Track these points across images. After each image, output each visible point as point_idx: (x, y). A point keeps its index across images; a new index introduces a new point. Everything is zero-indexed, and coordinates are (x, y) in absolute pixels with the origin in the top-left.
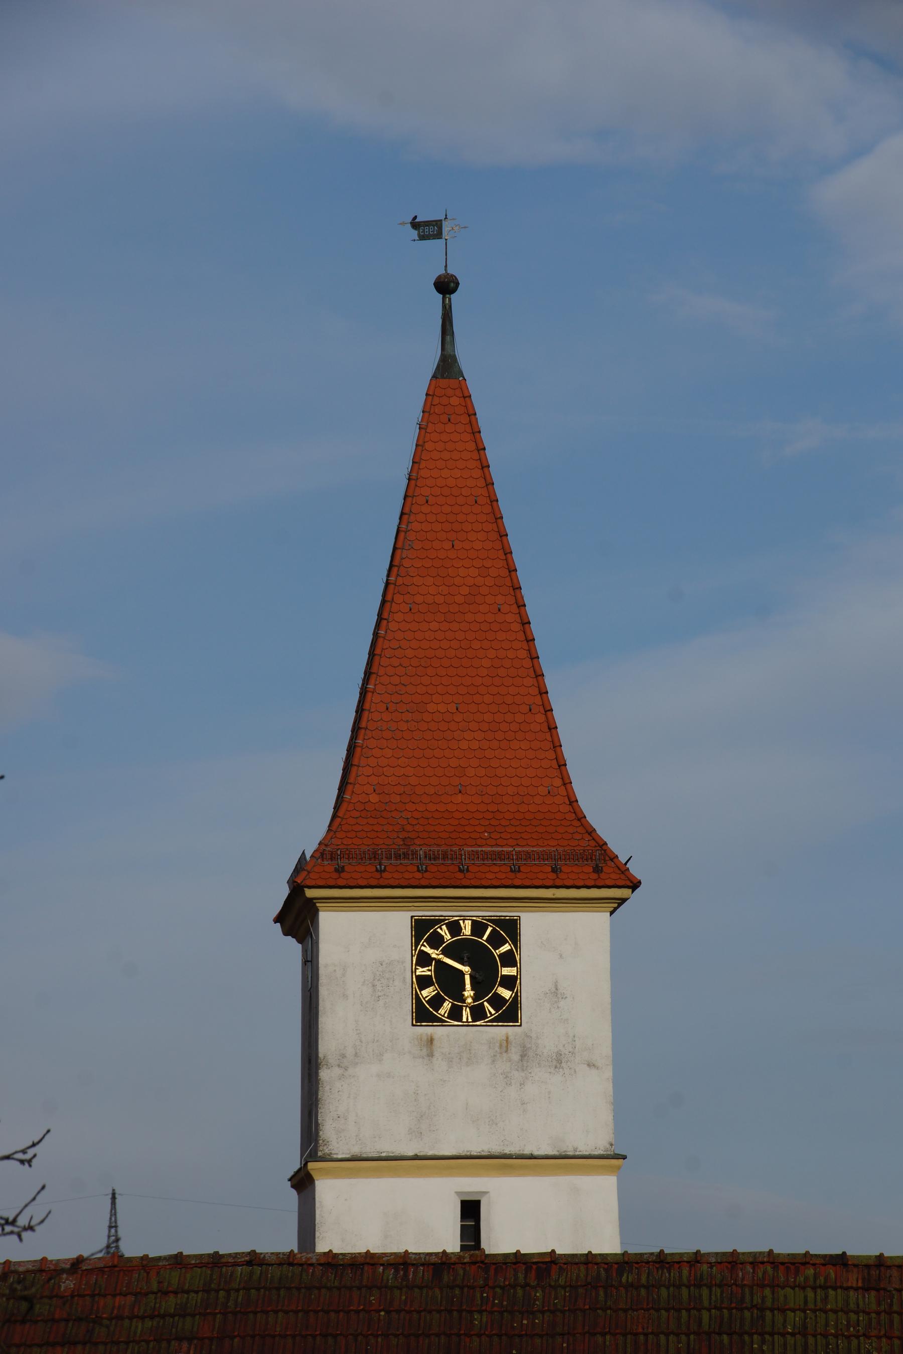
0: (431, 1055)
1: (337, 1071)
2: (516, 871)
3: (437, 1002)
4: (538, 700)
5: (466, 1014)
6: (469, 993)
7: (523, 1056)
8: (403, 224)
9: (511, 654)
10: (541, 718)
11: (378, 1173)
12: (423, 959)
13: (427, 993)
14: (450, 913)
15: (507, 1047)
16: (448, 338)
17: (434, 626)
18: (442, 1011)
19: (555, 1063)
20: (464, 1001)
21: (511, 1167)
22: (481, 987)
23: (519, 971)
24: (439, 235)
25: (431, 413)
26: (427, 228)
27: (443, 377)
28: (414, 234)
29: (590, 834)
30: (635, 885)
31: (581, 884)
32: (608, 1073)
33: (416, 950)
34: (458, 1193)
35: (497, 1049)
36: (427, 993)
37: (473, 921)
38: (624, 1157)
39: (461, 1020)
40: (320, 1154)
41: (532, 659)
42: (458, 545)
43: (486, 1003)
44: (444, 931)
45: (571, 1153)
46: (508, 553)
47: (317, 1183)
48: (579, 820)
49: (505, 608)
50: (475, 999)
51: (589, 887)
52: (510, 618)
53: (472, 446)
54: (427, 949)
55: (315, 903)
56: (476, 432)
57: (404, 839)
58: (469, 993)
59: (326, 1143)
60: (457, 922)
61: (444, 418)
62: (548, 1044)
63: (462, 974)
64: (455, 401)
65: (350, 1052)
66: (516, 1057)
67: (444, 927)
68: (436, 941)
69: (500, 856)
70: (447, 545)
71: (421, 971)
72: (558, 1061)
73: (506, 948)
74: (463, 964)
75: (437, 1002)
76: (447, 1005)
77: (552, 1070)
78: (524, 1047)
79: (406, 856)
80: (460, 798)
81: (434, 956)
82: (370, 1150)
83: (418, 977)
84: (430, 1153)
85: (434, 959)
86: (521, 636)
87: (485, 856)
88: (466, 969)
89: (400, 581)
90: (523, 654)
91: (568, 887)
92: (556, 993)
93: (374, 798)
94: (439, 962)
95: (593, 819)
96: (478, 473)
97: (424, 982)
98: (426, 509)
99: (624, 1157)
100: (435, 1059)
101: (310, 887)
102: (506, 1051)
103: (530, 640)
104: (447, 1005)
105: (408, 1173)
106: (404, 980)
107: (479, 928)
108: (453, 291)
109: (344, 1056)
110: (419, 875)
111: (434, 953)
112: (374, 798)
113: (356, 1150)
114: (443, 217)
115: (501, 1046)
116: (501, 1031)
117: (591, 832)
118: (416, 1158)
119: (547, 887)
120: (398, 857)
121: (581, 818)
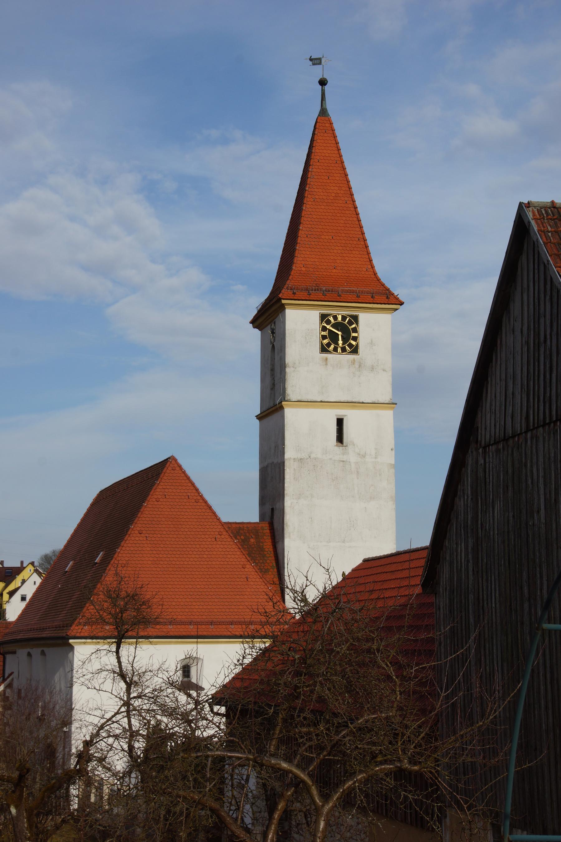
0: (326, 364)
1: (292, 369)
2: (358, 297)
3: (329, 345)
4: (361, 236)
5: (339, 350)
6: (340, 342)
7: (360, 366)
8: (306, 59)
9: (351, 219)
10: (363, 243)
11: (306, 407)
12: (324, 329)
13: (326, 341)
14: (334, 312)
16: (324, 102)
17: (323, 207)
18: (330, 348)
19: (371, 369)
20: (338, 345)
21: (355, 406)
22: (345, 340)
23: (358, 335)
24: (320, 63)
26: (315, 61)
27: (322, 116)
28: (311, 63)
29: (383, 285)
30: (402, 304)
31: (383, 302)
32: (390, 373)
34: (336, 415)
35: (350, 363)
36: (326, 341)
37: (342, 316)
38: (396, 404)
39: (337, 352)
40: (286, 399)
41: (359, 221)
42: (330, 178)
43: (346, 346)
44: (331, 319)
45: (377, 402)
46: (348, 182)
47: (285, 410)
48: (378, 280)
49: (348, 202)
50: (343, 344)
51: (385, 304)
52: (350, 206)
53: (334, 142)
54: (325, 325)
56: (335, 137)
57: (316, 284)
58: (340, 342)
59: (288, 395)
60: (336, 316)
61: (324, 131)
63: (338, 335)
64: (327, 125)
66: (357, 366)
67: (331, 317)
68: (328, 322)
69: (353, 292)
70: (327, 178)
71: (323, 333)
72: (372, 368)
73: (354, 326)
74: (338, 331)
75: (329, 345)
76: (332, 346)
79: (318, 290)
80: (335, 271)
81: (328, 328)
82: (304, 399)
83: (322, 335)
84: (326, 400)
85: (328, 329)
86: (354, 213)
87: (347, 291)
88: (340, 333)
89: (310, 190)
90: (356, 219)
91: (378, 304)
92: (372, 343)
93: (303, 269)
94: (330, 330)
95: (383, 280)
96: (336, 152)
98: (318, 164)
99: (396, 404)
101: (284, 299)
103: (358, 214)
104: (332, 346)
107: (344, 318)
108: (325, 85)
109: (295, 364)
110: (323, 297)
111: (328, 327)
112: (303, 269)
113: (299, 398)
114: (322, 57)
115: (352, 362)
116: (352, 357)
117: (383, 285)
118: (321, 402)
119: (370, 303)
120: (315, 290)
121: (379, 280)
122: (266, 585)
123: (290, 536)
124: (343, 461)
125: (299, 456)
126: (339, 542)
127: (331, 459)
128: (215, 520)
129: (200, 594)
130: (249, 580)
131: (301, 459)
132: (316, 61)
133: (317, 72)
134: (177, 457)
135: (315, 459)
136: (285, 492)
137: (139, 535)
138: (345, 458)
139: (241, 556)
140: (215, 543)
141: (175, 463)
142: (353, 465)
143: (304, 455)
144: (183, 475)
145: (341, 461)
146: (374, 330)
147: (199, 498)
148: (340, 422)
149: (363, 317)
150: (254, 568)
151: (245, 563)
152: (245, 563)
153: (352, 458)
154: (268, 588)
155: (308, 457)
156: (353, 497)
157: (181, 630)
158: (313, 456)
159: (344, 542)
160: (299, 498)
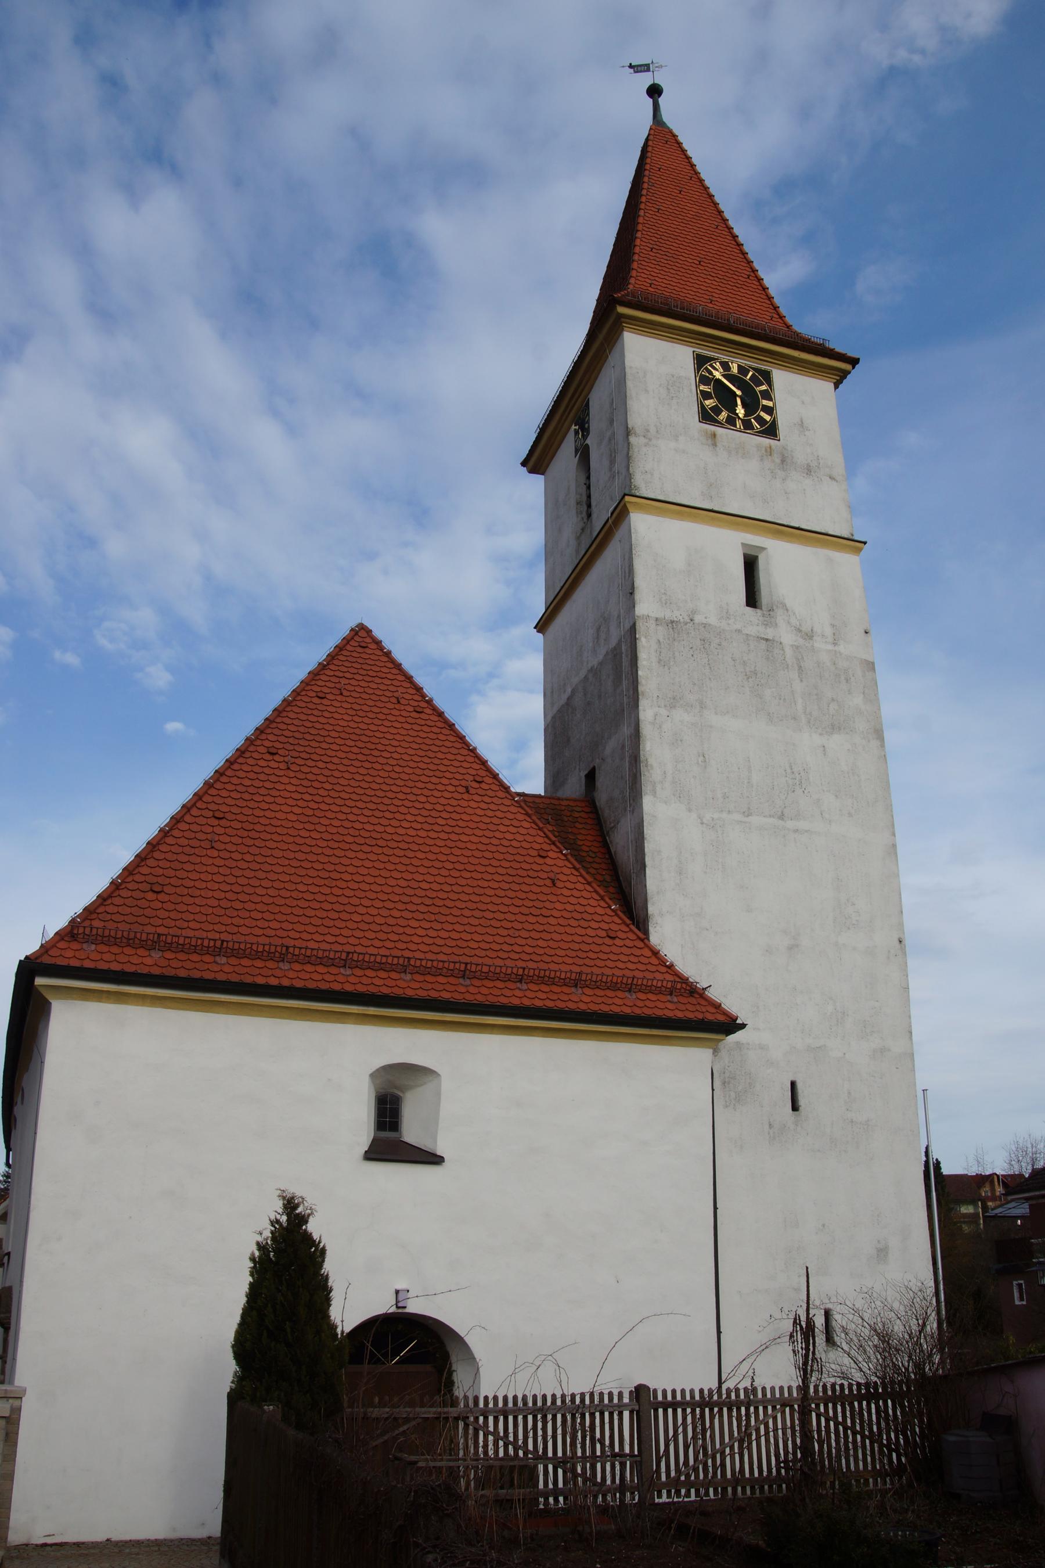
0: (715, 445)
1: (642, 440)
3: (717, 410)
5: (739, 423)
7: (783, 461)
11: (680, 516)
12: (704, 380)
13: (709, 403)
15: (771, 452)
21: (781, 533)
23: (775, 404)
25: (243, 755)
28: (632, 71)
33: (698, 373)
34: (744, 545)
35: (763, 452)
36: (709, 403)
43: (752, 420)
47: (631, 514)
55: (622, 323)
60: (727, 363)
62: (801, 456)
65: (653, 430)
66: (778, 461)
67: (718, 363)
73: (764, 387)
75: (717, 410)
77: (805, 475)
78: (783, 455)
88: (739, 393)
94: (718, 381)
97: (706, 395)
100: (718, 449)
102: (771, 455)
105: (703, 521)
106: (691, 391)
107: (743, 370)
109: (648, 431)
116: (766, 441)
122: (602, 898)
123: (654, 793)
124: (767, 640)
125: (668, 614)
126: (770, 816)
127: (739, 631)
128: (465, 752)
129: (428, 902)
130: (559, 884)
131: (672, 622)
132: (643, 68)
133: (646, 80)
134: (371, 1072)
135: (705, 625)
136: (641, 689)
137: (268, 757)
138: (770, 633)
139: (533, 832)
140: (466, 796)
141: (366, 635)
142: (789, 652)
143: (677, 615)
144: (385, 659)
145: (763, 639)
146: (803, 403)
147: (424, 705)
148: (751, 565)
149: (781, 378)
150: (568, 860)
151: (546, 847)
152: (546, 847)
153: (787, 637)
154: (610, 907)
155: (687, 619)
156: (795, 718)
157: (377, 981)
158: (698, 619)
159: (782, 817)
160: (673, 707)
